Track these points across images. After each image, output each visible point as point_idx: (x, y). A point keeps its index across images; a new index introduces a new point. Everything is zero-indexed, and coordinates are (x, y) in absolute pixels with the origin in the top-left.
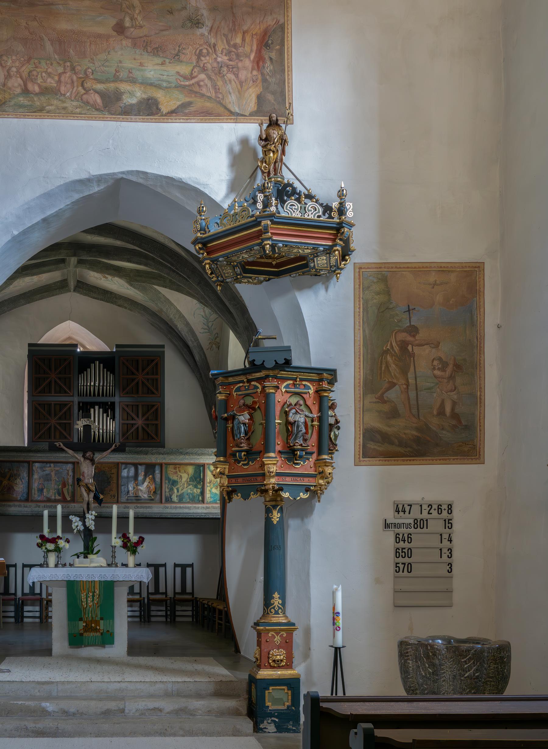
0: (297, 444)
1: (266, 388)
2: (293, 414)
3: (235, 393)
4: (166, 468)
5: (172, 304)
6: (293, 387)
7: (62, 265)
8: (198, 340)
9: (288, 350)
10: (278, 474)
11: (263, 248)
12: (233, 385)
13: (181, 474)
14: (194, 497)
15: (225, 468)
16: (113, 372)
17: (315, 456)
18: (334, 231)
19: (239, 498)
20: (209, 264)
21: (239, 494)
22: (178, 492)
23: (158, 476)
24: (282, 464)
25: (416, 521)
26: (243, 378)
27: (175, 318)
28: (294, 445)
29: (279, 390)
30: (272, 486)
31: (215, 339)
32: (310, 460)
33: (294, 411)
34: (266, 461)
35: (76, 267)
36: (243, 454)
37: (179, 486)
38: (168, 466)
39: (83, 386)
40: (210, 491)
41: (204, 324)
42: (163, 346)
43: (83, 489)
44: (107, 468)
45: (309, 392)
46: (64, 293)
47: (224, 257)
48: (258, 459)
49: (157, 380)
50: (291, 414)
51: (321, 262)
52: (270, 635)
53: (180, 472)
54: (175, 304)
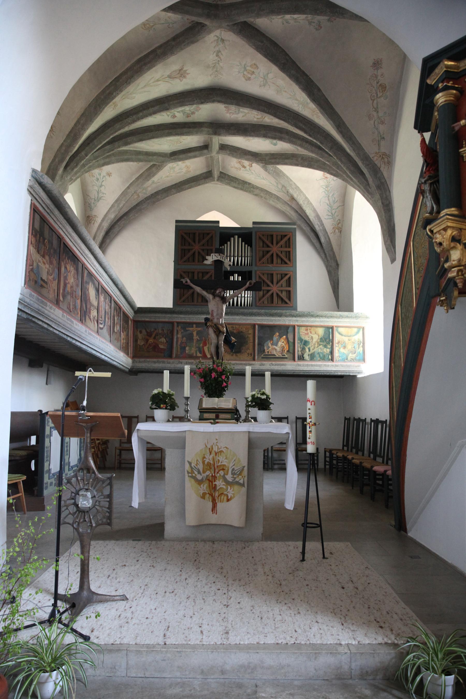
4: (299, 329)
5: (302, 192)
7: (205, 151)
8: (323, 225)
14: (324, 356)
15: (461, 229)
16: (250, 244)
22: (309, 351)
31: (338, 225)
35: (218, 153)
37: (310, 346)
40: (338, 351)
43: (211, 331)
49: (289, 252)
53: (311, 333)
54: (304, 192)
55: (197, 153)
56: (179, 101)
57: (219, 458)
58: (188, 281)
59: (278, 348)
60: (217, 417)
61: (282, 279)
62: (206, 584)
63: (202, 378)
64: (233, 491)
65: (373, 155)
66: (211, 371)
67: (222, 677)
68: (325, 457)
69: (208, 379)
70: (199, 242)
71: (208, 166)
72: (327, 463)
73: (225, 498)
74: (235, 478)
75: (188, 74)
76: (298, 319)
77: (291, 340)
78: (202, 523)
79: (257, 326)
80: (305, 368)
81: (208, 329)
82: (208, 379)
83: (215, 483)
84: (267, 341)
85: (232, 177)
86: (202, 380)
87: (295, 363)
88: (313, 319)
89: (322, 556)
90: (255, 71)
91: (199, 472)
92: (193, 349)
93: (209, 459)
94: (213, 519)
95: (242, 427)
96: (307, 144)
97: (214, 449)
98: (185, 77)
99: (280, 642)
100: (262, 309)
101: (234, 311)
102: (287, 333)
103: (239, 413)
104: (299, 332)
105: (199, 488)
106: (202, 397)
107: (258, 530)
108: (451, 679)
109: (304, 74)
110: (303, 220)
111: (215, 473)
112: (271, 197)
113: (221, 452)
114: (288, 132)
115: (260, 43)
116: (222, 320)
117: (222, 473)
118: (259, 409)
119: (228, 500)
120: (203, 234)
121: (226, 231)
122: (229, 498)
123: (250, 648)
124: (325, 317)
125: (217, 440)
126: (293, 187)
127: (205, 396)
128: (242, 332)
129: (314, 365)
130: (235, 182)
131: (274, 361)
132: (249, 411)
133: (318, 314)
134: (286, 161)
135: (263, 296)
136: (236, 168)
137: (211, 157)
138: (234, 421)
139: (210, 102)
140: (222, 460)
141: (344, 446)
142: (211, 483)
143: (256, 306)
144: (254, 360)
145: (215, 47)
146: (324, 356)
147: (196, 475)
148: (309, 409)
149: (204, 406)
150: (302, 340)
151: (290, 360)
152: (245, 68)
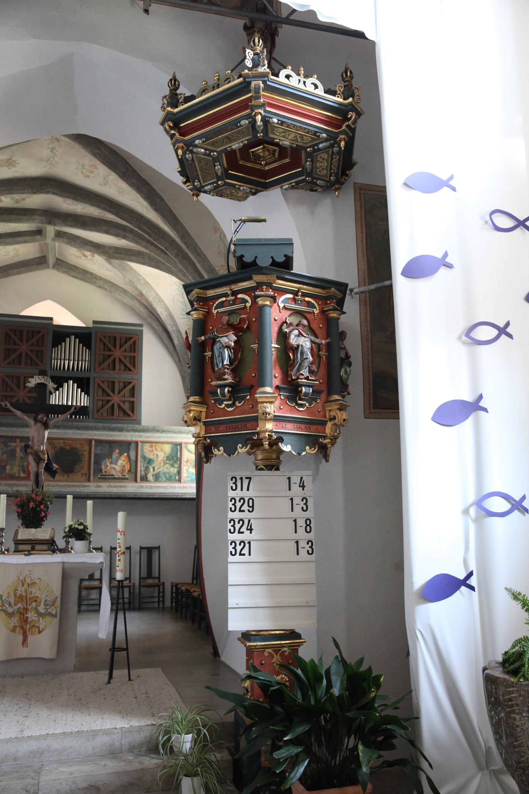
0: (301, 377)
1: (258, 299)
2: (296, 336)
3: (216, 311)
4: (142, 446)
5: (152, 288)
6: (293, 303)
7: (38, 237)
8: (177, 325)
9: (289, 243)
10: (277, 419)
11: (255, 121)
12: (212, 301)
13: (158, 453)
14: (171, 477)
15: (201, 412)
16: (89, 347)
17: (324, 396)
18: (340, 116)
19: (220, 453)
20: (182, 148)
21: (221, 448)
22: (154, 470)
23: (132, 454)
24: (281, 404)
25: (308, 522)
26: (225, 289)
27: (154, 301)
28: (298, 378)
29: (275, 305)
30: (268, 435)
32: (318, 401)
33: (296, 332)
34: (259, 397)
35: (53, 240)
36: (226, 390)
37: (155, 465)
38: (144, 444)
39: (57, 359)
40: (187, 470)
41: (183, 310)
42: (141, 326)
43: (31, 459)
44: (79, 445)
45: (313, 312)
46: (42, 269)
47: (201, 139)
48: (248, 398)
49: (134, 357)
50: (292, 336)
51: (321, 164)
52: (266, 654)
53: (156, 450)
54: (155, 288)
55: (28, 238)
56: (6, 188)
57: (32, 590)
58: (8, 404)
59: (118, 468)
60: (33, 549)
61: (125, 387)
62: (9, 706)
63: (18, 508)
64: (45, 622)
65: (219, 268)
66: (30, 499)
67: (15, 763)
68: (172, 592)
69: (26, 508)
70: (27, 342)
71: (42, 250)
72: (174, 600)
73: (37, 630)
74: (47, 609)
75: (18, 164)
76: (142, 434)
77: (133, 458)
78: (11, 658)
79: (93, 442)
80: (149, 491)
81: (28, 456)
82: (26, 508)
83: (27, 615)
84: (105, 459)
85: (71, 265)
86: (19, 510)
87: (137, 485)
88: (158, 435)
89: (128, 679)
90: (94, 170)
91: (10, 605)
92: (15, 467)
93: (21, 591)
94: (23, 653)
95: (58, 558)
96: (153, 247)
97: (27, 581)
98: (14, 166)
99: (66, 731)
100: (100, 423)
101: (66, 424)
102: (129, 449)
103: (56, 544)
104: (142, 449)
105: (10, 621)
106: (18, 528)
107: (71, 660)
108: (189, 737)
109: (146, 183)
110: (154, 317)
111: (27, 605)
112: (117, 290)
113: (34, 583)
114: (132, 231)
115: (98, 151)
116: (43, 447)
117: (34, 605)
118: (76, 540)
119: (40, 632)
120: (33, 332)
121: (60, 330)
122: (41, 629)
123: (39, 737)
124: (173, 432)
125: (30, 571)
126: (141, 282)
127: (22, 527)
128: (75, 448)
129: (159, 487)
130: (75, 271)
131: (113, 482)
132: (69, 542)
133: (165, 429)
134: (133, 258)
135: (102, 407)
136: (76, 256)
137: (45, 243)
138: (50, 552)
139: (44, 193)
140: (35, 591)
141: (193, 579)
142: (22, 616)
143: (93, 418)
144: (89, 480)
145: (48, 145)
146: (171, 477)
147: (6, 608)
148: (119, 539)
149: (20, 537)
150: (146, 458)
151: (131, 481)
152: (83, 166)
